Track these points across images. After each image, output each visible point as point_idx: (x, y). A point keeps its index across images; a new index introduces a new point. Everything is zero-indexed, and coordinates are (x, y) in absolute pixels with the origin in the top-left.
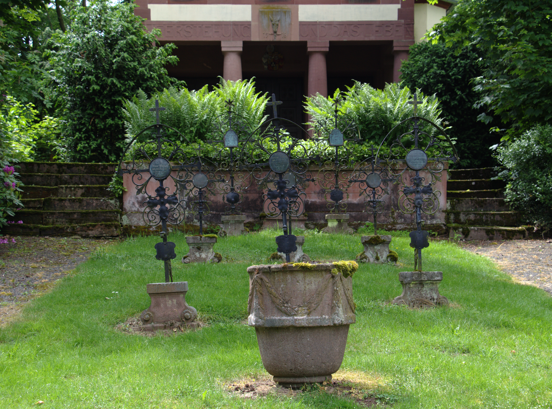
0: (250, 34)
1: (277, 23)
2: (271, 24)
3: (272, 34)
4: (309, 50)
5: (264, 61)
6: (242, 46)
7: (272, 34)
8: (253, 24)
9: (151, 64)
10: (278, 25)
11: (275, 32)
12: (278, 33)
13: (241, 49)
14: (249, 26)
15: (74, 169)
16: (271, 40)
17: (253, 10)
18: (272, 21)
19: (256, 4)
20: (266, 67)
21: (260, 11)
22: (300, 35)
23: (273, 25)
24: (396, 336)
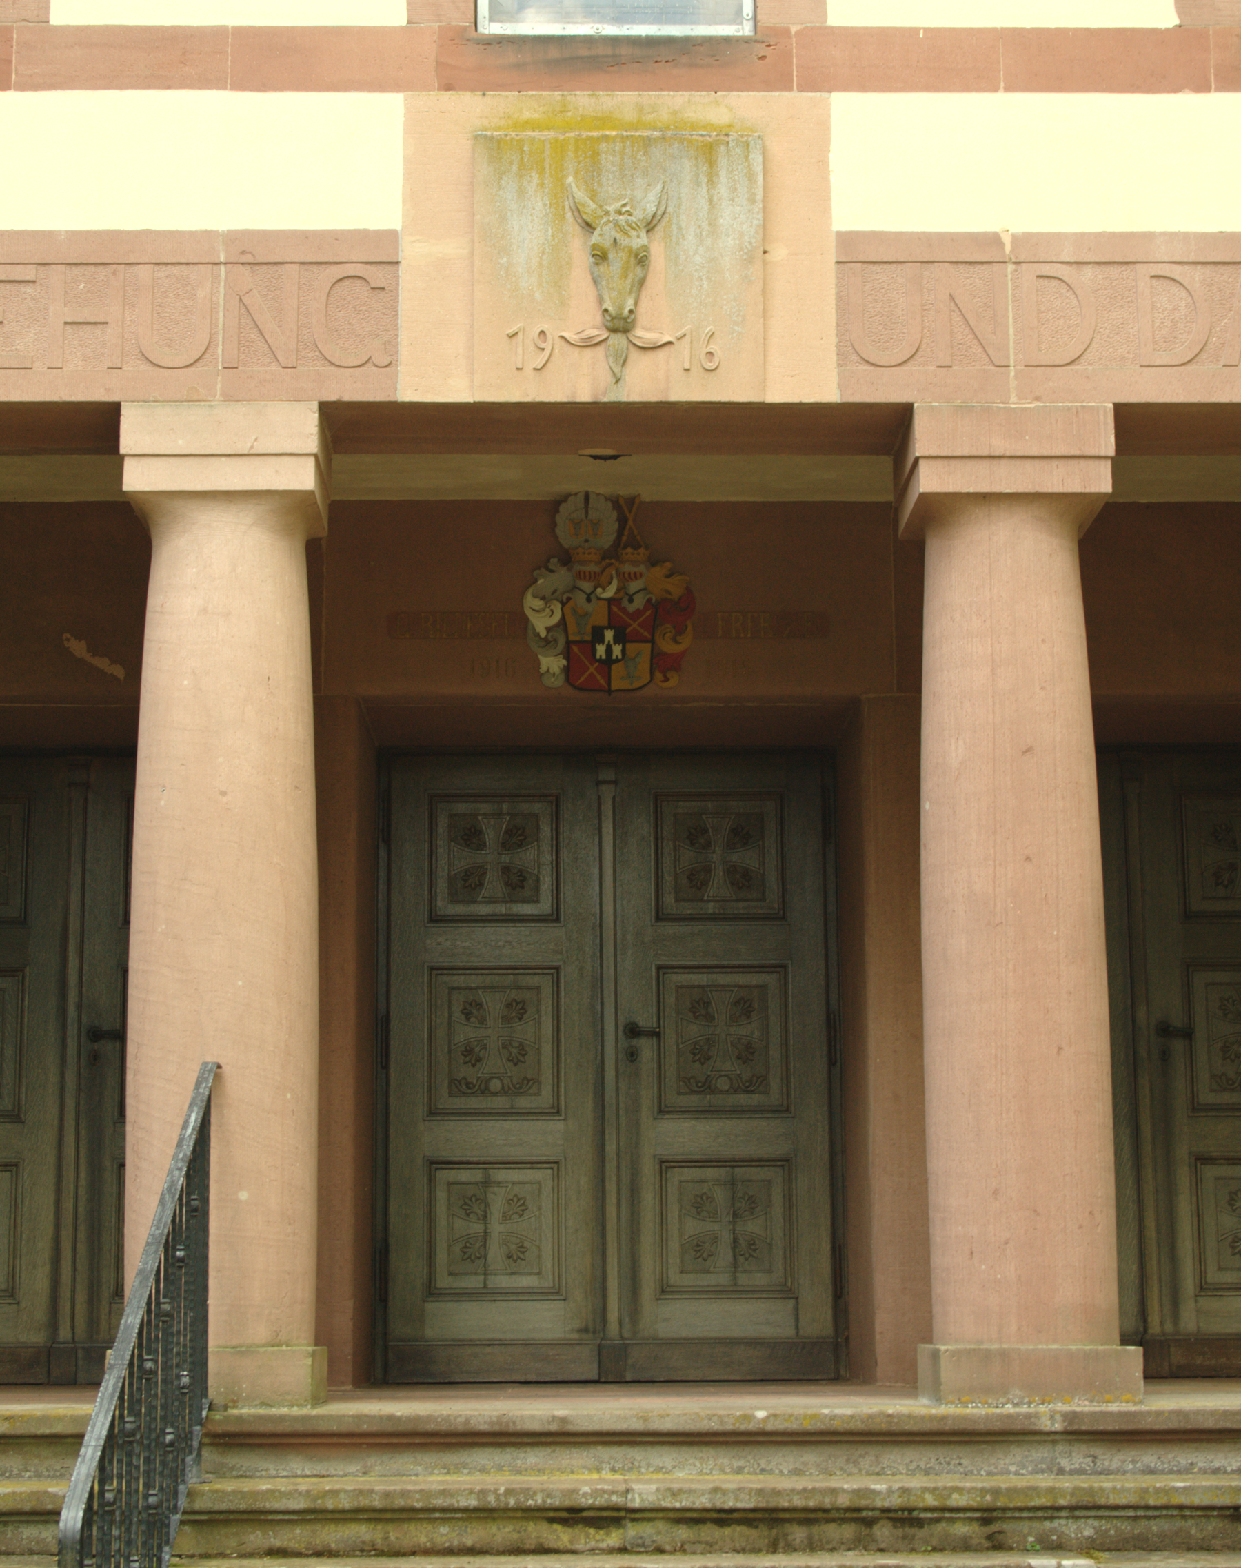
0: (391, 346)
1: (638, 240)
2: (578, 249)
3: (589, 344)
4: (929, 480)
5: (542, 620)
6: (312, 443)
7: (589, 344)
8: (412, 252)
9: (938, 1350)
10: (641, 259)
11: (620, 325)
12: (643, 334)
13: (303, 477)
14: (377, 276)
15: (137, 1396)
16: (584, 395)
17: (414, 126)
18: (589, 227)
19: (448, 87)
20: (552, 663)
21: (476, 138)
22: (848, 352)
23: (600, 256)
24: (757, 1426)
